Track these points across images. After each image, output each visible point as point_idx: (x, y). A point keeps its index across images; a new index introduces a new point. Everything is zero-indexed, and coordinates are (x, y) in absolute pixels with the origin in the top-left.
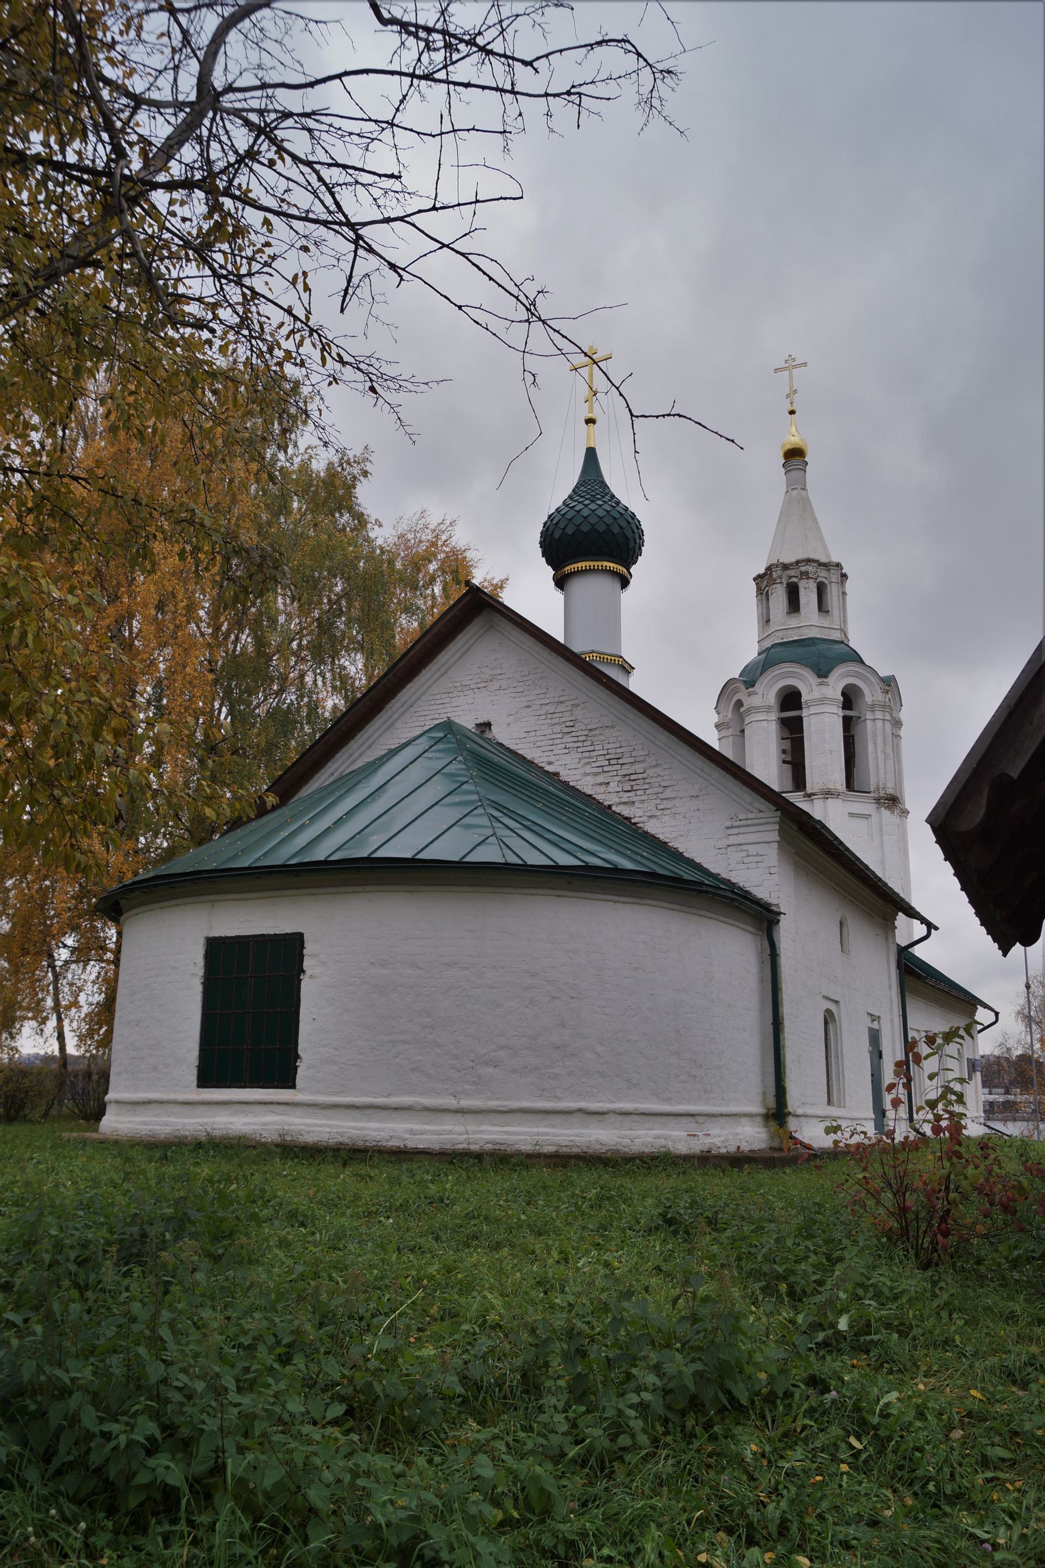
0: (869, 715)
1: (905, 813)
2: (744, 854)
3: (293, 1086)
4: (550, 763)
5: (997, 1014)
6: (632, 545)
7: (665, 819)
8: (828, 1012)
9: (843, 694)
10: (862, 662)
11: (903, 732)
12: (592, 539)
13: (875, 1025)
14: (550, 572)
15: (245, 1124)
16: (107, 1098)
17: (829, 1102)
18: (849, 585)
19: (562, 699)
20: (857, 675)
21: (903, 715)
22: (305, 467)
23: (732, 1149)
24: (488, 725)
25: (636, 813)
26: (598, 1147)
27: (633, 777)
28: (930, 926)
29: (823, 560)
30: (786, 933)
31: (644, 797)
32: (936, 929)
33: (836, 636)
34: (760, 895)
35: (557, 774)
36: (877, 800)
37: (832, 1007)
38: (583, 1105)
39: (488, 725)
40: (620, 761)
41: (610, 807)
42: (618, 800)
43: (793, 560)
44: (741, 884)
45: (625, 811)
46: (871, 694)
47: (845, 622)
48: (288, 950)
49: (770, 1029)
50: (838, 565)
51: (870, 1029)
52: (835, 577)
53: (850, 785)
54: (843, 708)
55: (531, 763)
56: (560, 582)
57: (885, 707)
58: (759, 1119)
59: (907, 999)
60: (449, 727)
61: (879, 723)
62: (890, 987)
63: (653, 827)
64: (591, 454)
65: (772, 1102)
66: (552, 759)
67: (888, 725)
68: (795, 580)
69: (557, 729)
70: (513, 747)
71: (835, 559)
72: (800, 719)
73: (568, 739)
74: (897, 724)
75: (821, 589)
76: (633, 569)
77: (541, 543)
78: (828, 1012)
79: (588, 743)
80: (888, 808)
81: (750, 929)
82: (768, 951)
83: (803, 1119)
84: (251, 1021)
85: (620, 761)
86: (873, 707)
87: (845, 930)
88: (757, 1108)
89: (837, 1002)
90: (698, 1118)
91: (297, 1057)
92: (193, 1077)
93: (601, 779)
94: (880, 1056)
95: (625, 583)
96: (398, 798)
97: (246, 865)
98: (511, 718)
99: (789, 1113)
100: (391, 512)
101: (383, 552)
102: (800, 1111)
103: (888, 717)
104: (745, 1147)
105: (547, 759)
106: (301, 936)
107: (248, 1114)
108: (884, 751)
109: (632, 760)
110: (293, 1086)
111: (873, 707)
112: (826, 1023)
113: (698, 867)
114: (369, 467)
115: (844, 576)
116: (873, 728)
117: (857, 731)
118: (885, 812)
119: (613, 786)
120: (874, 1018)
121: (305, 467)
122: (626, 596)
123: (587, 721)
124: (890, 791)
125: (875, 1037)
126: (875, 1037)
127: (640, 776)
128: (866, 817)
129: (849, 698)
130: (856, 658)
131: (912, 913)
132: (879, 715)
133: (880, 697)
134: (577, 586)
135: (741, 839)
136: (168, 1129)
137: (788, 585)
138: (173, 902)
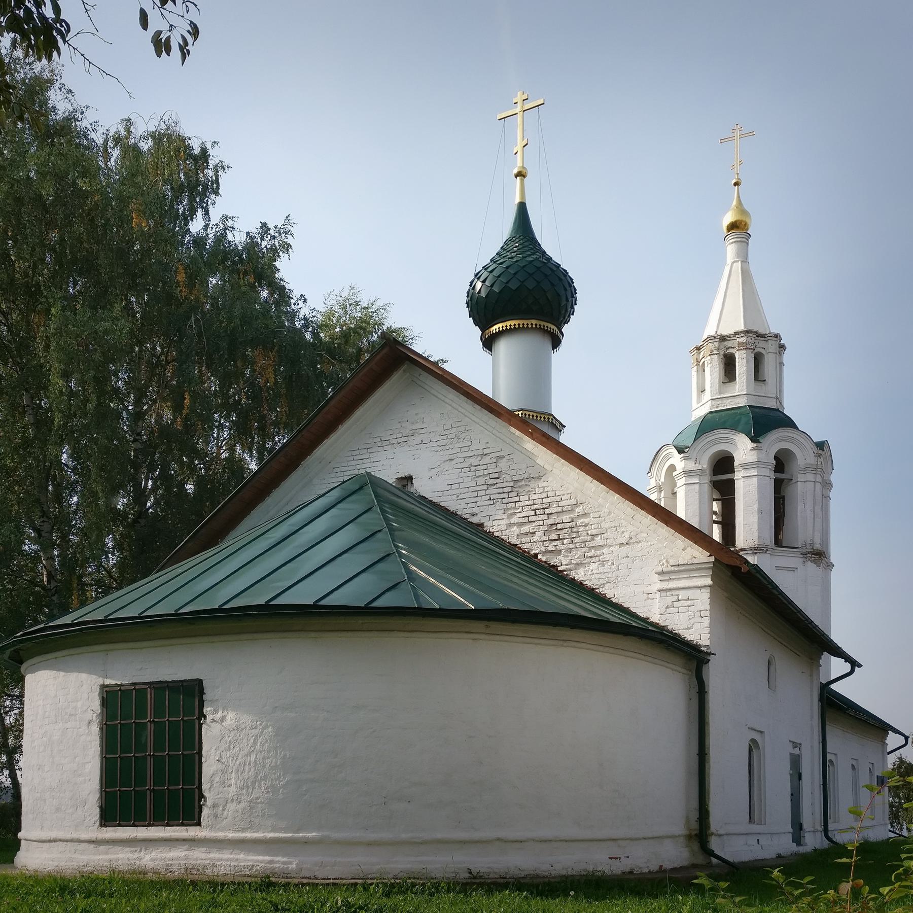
0: (801, 477)
1: (830, 566)
2: (675, 598)
3: (199, 824)
4: (474, 515)
5: (907, 738)
6: (564, 303)
7: (593, 566)
8: (753, 741)
9: (776, 458)
10: (796, 428)
11: (832, 494)
12: (526, 294)
13: (796, 751)
14: (477, 332)
15: (152, 860)
16: (20, 835)
17: (751, 819)
18: (787, 356)
19: (486, 451)
20: (791, 440)
21: (833, 478)
22: (221, 238)
23: (654, 867)
24: (409, 479)
25: (562, 562)
26: (517, 872)
27: (559, 526)
28: (854, 664)
29: (761, 331)
30: (714, 674)
31: (571, 546)
32: (860, 666)
33: (771, 404)
34: (689, 638)
35: (482, 525)
36: (804, 554)
37: (757, 737)
38: (502, 834)
39: (409, 479)
40: (547, 511)
41: (536, 555)
42: (543, 549)
43: (733, 332)
44: (670, 628)
45: (554, 561)
46: (804, 457)
47: (781, 391)
48: (190, 695)
49: (607, 639)
50: (777, 336)
51: (791, 755)
52: (772, 346)
53: (778, 542)
54: (775, 471)
55: (454, 515)
56: (489, 343)
57: (816, 469)
58: (682, 839)
59: (828, 727)
60: (367, 483)
61: (810, 485)
62: (812, 717)
63: (579, 575)
64: (522, 209)
65: (695, 826)
66: (476, 510)
67: (818, 486)
68: (731, 351)
69: (481, 481)
70: (435, 500)
71: (774, 331)
72: (732, 482)
73: (492, 490)
74: (827, 485)
75: (758, 360)
76: (566, 329)
77: (467, 303)
78: (753, 741)
79: (514, 494)
80: (814, 562)
81: (679, 669)
82: (697, 689)
83: (725, 837)
84: (151, 768)
85: (547, 511)
86: (805, 470)
87: (772, 668)
88: (679, 829)
89: (761, 732)
90: (620, 842)
91: (202, 796)
92: (94, 812)
93: (525, 529)
94: (800, 777)
95: (556, 342)
96: (298, 546)
97: (132, 612)
98: (434, 472)
99: (712, 834)
100: (316, 284)
101: (306, 326)
102: (721, 832)
103: (819, 479)
104: (668, 865)
105: (470, 511)
106: (200, 682)
107: (155, 850)
108: (814, 511)
109: (560, 509)
110: (199, 824)
111: (805, 470)
112: (750, 750)
113: (627, 611)
114: (290, 240)
115: (782, 347)
116: (803, 488)
117: (788, 492)
118: (811, 566)
119: (539, 536)
120: (796, 745)
121: (221, 238)
122: (558, 358)
123: (513, 473)
124: (818, 546)
125: (795, 762)
126: (795, 762)
127: (568, 525)
128: (793, 569)
129: (781, 463)
130: (789, 423)
131: (837, 652)
132: (810, 477)
133: (811, 460)
134: (502, 346)
135: (672, 585)
136: (74, 864)
137: (725, 356)
138: (65, 652)
